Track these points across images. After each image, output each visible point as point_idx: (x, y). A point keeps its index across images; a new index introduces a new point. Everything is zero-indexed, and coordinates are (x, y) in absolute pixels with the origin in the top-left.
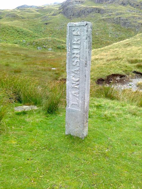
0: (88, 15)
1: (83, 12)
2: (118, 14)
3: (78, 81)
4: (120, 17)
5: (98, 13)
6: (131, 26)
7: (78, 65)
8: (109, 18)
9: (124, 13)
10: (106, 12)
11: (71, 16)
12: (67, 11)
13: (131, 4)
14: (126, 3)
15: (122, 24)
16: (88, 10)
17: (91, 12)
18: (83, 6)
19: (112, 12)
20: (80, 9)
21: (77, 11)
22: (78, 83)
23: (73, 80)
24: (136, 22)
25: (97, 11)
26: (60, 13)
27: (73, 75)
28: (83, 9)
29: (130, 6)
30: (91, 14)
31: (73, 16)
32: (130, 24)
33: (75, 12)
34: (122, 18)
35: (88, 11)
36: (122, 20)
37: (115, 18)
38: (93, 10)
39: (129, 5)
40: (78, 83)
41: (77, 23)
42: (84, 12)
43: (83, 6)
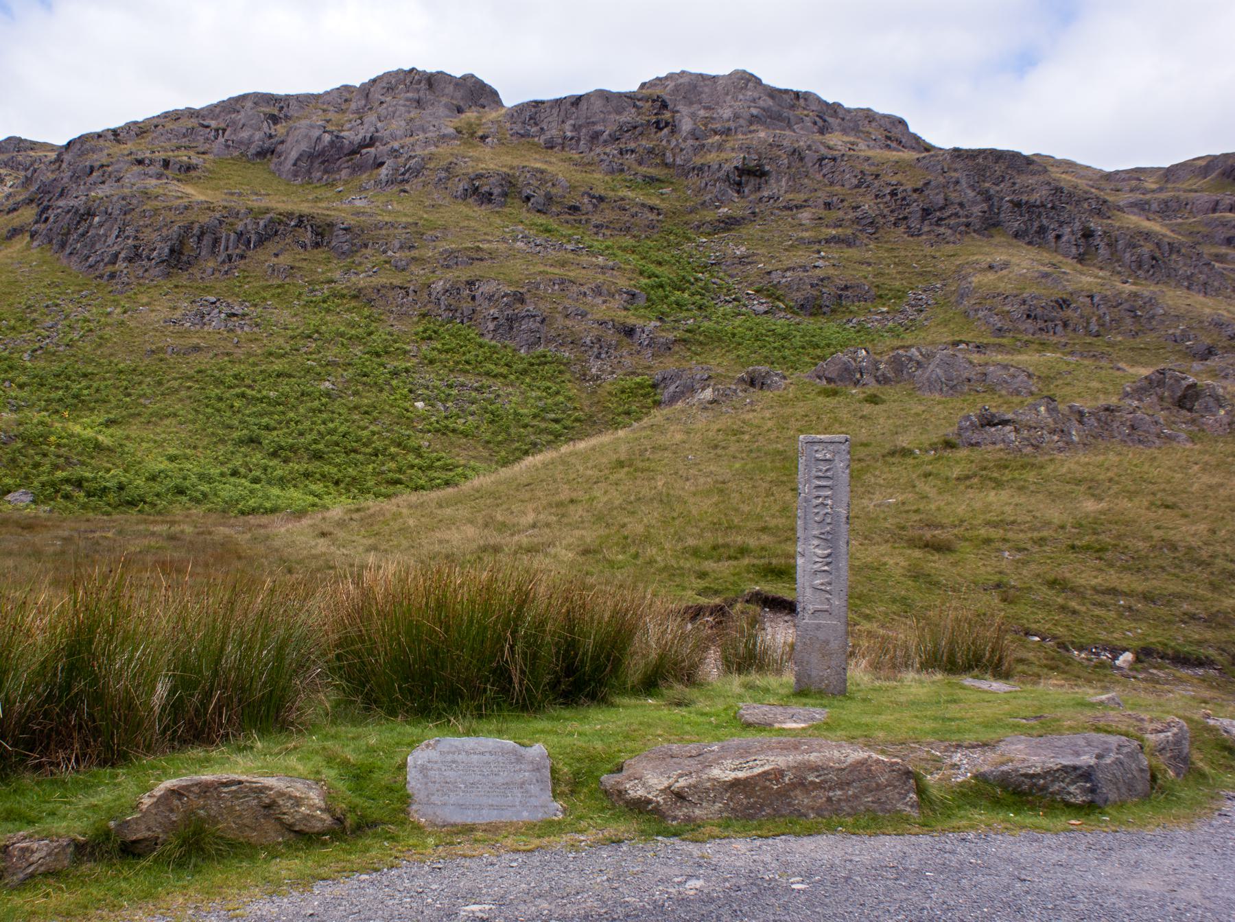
0: (242, 257)
1: (207, 240)
2: (450, 259)
3: (829, 555)
4: (470, 283)
5: (317, 245)
6: (548, 341)
7: (829, 521)
8: (397, 282)
9: (492, 255)
10: (366, 246)
11: (121, 265)
12: (84, 225)
13: (528, 198)
14: (497, 191)
15: (491, 326)
16: (240, 227)
17: (262, 240)
18: (195, 193)
19: (411, 247)
20: (181, 221)
21: (165, 232)
22: (829, 560)
23: (815, 554)
24: (584, 315)
25: (308, 237)
26: (15, 232)
27: (816, 542)
28: (204, 219)
29: (524, 214)
30: (264, 257)
31: (130, 260)
32: (544, 329)
33: (149, 235)
34: (486, 288)
35: (240, 235)
36: (490, 298)
37: (439, 286)
38: (273, 230)
39: (518, 202)
40: (829, 560)
41: (822, 437)
42: (216, 241)
43: (195, 193)
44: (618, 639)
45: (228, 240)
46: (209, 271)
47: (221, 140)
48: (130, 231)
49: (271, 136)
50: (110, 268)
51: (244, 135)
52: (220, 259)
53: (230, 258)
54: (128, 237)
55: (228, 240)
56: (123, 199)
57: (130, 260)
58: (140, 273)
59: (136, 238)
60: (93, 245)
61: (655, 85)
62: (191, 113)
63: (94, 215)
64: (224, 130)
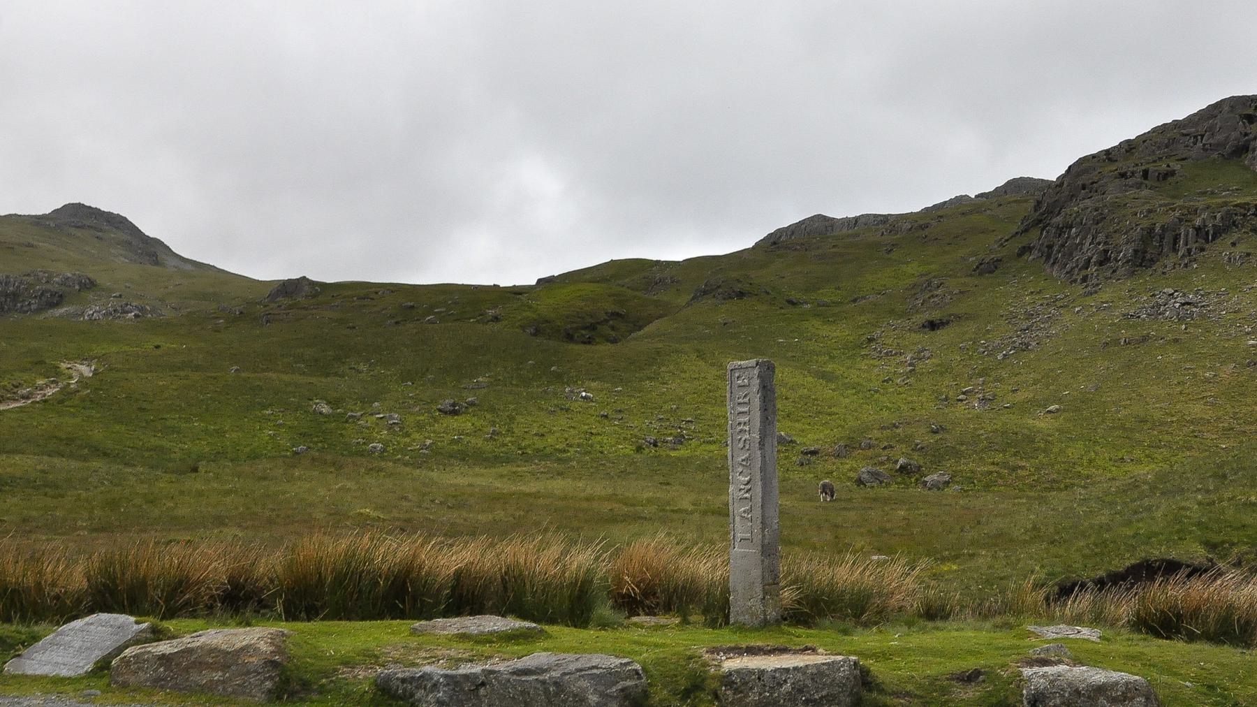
0: (1202, 250)
3: (748, 482)
11: (1093, 269)
16: (1198, 222)
31: (1100, 264)
42: (1176, 239)
44: (943, 608)
45: (1187, 236)
46: (1170, 265)
47: (1200, 145)
48: (1101, 237)
49: (1246, 135)
50: (1084, 273)
51: (1220, 137)
52: (1180, 254)
53: (1189, 251)
54: (1099, 244)
55: (1187, 236)
56: (1096, 210)
57: (1101, 263)
58: (1108, 274)
59: (1106, 243)
60: (1071, 254)
61: (1086, 171)
62: (1176, 124)
63: (1071, 227)
64: (1202, 136)
